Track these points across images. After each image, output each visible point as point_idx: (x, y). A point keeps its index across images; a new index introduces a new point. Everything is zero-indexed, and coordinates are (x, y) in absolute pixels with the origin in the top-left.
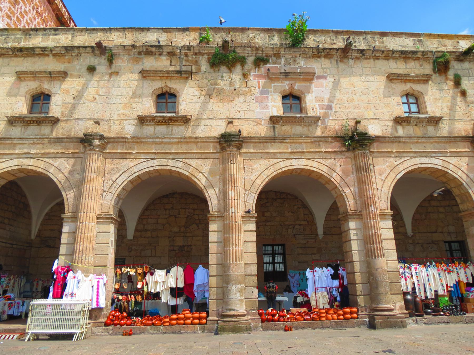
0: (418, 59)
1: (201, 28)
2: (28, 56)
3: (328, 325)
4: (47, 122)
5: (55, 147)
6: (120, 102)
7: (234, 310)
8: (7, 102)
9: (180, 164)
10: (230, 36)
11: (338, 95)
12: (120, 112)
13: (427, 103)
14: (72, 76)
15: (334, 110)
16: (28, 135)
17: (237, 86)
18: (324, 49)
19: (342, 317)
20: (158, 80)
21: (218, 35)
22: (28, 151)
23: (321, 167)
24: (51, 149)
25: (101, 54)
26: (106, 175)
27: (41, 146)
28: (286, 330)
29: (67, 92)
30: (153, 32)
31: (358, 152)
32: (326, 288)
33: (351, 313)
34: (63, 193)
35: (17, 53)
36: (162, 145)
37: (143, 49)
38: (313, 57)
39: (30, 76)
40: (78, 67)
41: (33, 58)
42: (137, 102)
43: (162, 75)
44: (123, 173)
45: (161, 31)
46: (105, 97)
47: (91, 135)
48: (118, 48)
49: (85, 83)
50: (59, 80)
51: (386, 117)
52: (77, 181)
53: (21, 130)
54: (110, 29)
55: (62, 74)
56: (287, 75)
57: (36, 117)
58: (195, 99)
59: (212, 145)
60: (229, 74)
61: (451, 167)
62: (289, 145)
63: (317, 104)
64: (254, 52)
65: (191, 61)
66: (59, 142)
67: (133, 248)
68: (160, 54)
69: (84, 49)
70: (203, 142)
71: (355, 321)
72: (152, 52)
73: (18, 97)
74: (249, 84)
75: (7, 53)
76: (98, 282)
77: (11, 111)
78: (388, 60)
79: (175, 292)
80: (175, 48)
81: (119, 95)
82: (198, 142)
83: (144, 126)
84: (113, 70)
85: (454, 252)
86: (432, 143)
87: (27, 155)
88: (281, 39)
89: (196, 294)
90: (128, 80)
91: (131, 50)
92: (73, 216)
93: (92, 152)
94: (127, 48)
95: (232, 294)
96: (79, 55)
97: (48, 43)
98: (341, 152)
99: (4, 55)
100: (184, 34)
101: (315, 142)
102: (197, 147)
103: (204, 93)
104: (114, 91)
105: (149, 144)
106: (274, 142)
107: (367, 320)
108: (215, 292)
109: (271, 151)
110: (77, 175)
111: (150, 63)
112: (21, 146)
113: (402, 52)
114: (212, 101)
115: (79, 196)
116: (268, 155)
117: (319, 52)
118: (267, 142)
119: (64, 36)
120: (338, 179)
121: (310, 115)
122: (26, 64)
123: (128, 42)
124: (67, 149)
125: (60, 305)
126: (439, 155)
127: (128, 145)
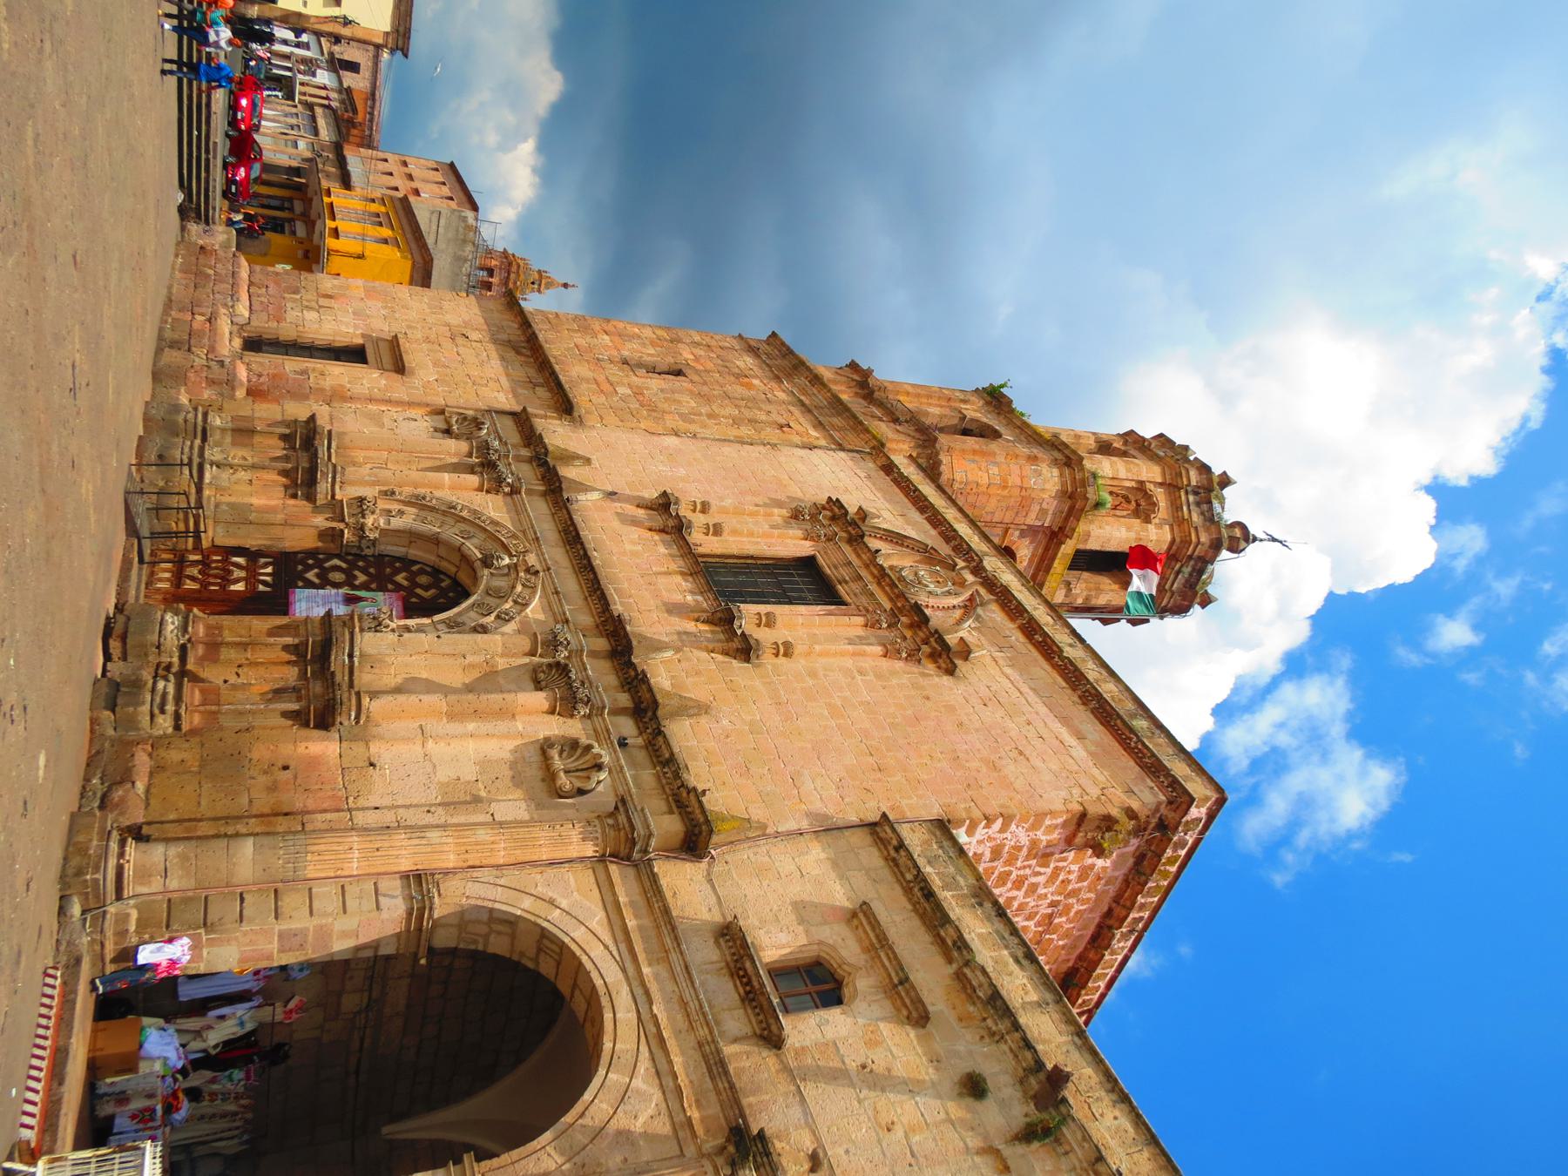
2: (922, 916)
14: (925, 1040)
25: (1034, 1097)
47: (768, 1154)
48: (1084, 1139)
49: (924, 1081)
50: (898, 1010)
52: (599, 1165)
57: (762, 985)
66: (710, 1071)
69: (1022, 1044)
84: (1007, 1151)
99: (897, 865)
110: (619, 1159)
112: (665, 974)
124: (697, 1101)
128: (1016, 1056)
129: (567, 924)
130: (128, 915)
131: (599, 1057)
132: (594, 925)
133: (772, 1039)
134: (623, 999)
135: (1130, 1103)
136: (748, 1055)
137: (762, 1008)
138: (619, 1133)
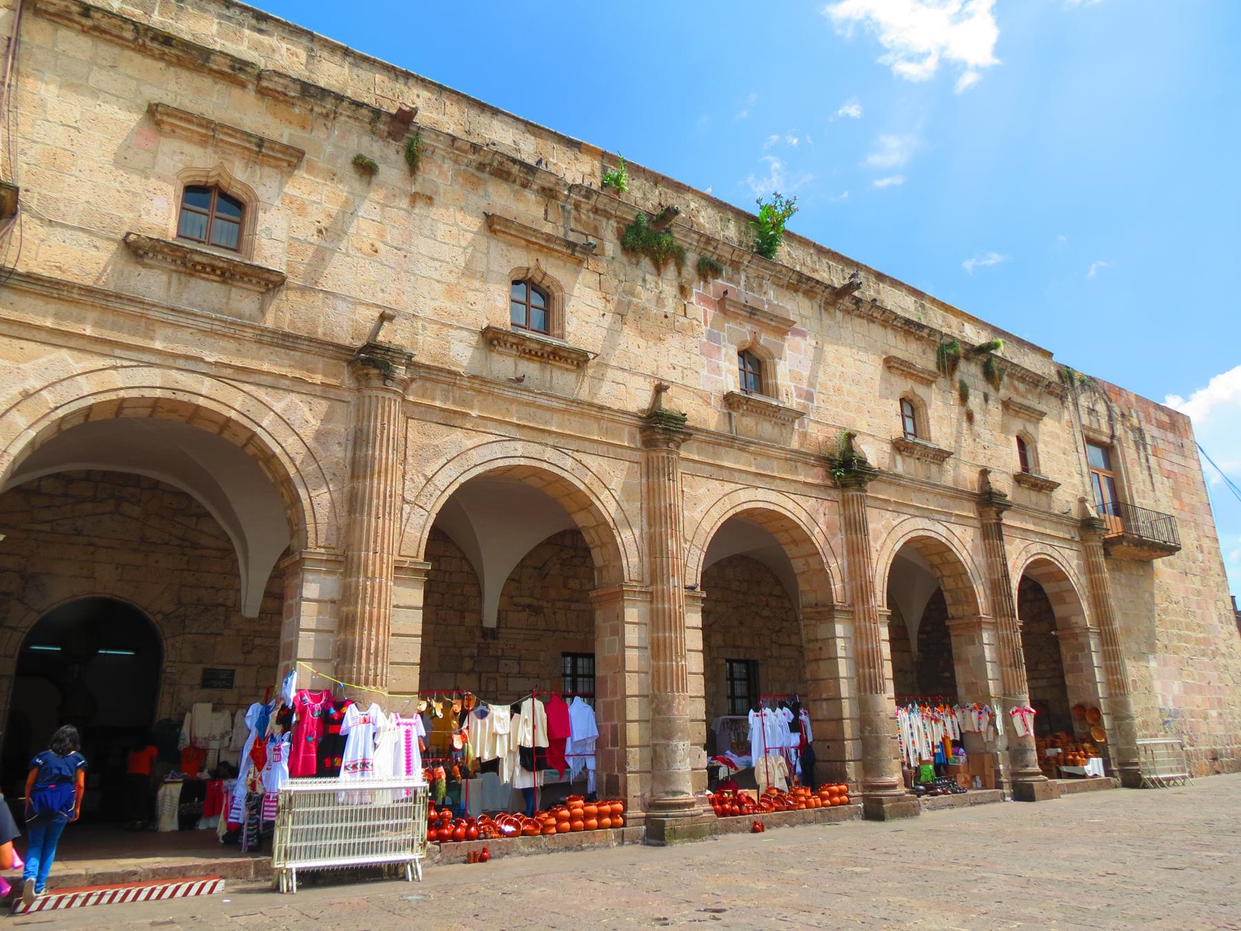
0: (920, 338)
1: (605, 153)
2: (179, 63)
3: (812, 818)
4: (254, 281)
5: (273, 357)
6: (436, 276)
7: (683, 793)
8: (118, 186)
9: (568, 463)
10: (657, 193)
11: (822, 377)
12: (437, 303)
13: (931, 422)
14: (311, 169)
15: (816, 404)
16: (191, 304)
17: (669, 309)
18: (809, 279)
19: (827, 802)
20: (522, 247)
21: (636, 183)
22: (193, 351)
23: (798, 511)
24: (262, 360)
25: (390, 134)
26: (410, 460)
27: (232, 345)
28: (755, 830)
29: (302, 210)
30: (507, 123)
31: (852, 493)
32: (781, 749)
33: (841, 793)
34: (302, 492)
35: (148, 43)
36: (532, 410)
37: (492, 160)
38: (788, 287)
39: (195, 128)
40: (329, 149)
41: (194, 75)
42: (477, 290)
43: (534, 240)
44: (449, 461)
45: (522, 127)
46: (402, 253)
47: (388, 350)
48: (438, 136)
49: (347, 199)
50: (276, 167)
51: (883, 436)
52: (337, 463)
53: (170, 283)
54: (407, 76)
55: (292, 155)
56: (752, 313)
57: (229, 261)
58: (595, 317)
59: (627, 429)
60: (655, 278)
61: (956, 542)
62: (752, 458)
63: (793, 385)
64: (702, 245)
65: (586, 225)
66: (287, 347)
67: (258, 641)
68: (524, 186)
69: (353, 107)
70: (613, 421)
71: (846, 807)
72: (509, 173)
73: (152, 180)
74: (690, 309)
75: (115, 32)
76: (408, 732)
77: (131, 215)
78: (885, 327)
79: (530, 758)
80: (562, 183)
81: (433, 259)
82: (603, 418)
83: (493, 354)
84: (416, 188)
85: (580, 679)
86: (936, 494)
87: (191, 363)
88: (740, 232)
89: (570, 762)
90: (451, 229)
91: (466, 152)
92: (333, 558)
93: (388, 395)
94: (458, 144)
95: (678, 759)
96: (332, 116)
97: (241, 48)
98: (826, 487)
99: (104, 32)
100: (570, 154)
101: (791, 460)
102: (600, 429)
103: (611, 306)
104: (422, 245)
105: (505, 399)
106: (732, 447)
107: (861, 805)
108: (637, 757)
109: (726, 464)
110: (336, 448)
111: (502, 198)
112: (169, 331)
113: (908, 322)
114: (626, 329)
115: (354, 503)
116: (721, 473)
117: (799, 281)
118: (719, 444)
119: (285, 45)
120: (821, 538)
121: (255, 263)
122: (173, 86)
123: (452, 126)
124: (308, 370)
125: (334, 794)
126: (943, 518)
127: (457, 393)
128: (356, 119)
129: (67, 392)
131: (490, 471)
133: (270, 283)
134: (187, 381)
135: (413, 75)
136: (278, 309)
137: (246, 274)
138: (316, 439)
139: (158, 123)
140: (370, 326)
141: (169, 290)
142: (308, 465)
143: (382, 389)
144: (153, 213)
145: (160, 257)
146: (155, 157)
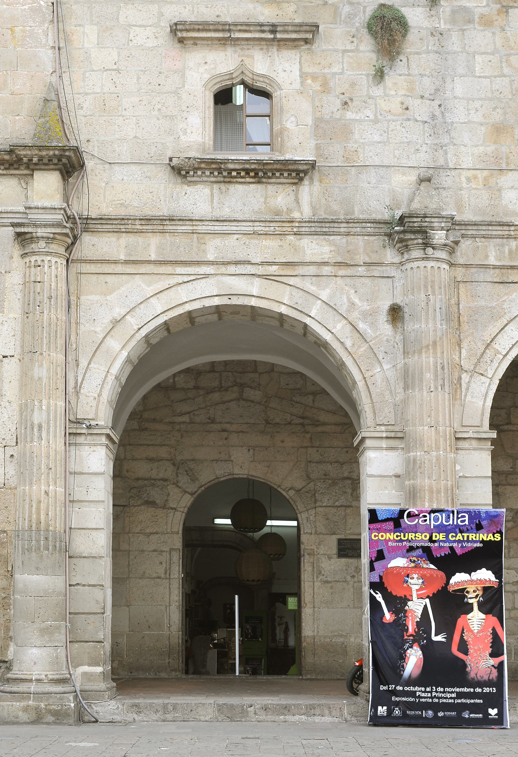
4: (286, 174)
53: (212, 195)
55: (306, 32)
66: (325, 234)
130: (85, 674)
132: (150, 290)
133: (297, 173)
139: (181, 41)
140: (407, 192)
141: (212, 202)
142: (359, 347)
143: (423, 259)
144: (188, 131)
145: (199, 173)
146: (183, 76)
